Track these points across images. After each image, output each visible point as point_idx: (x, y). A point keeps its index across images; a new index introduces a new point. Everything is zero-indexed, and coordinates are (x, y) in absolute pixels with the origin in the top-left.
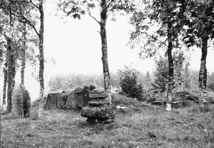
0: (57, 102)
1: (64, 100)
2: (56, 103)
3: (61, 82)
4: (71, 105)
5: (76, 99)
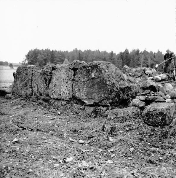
0: (32, 83)
1: (46, 81)
2: (31, 86)
3: (37, 56)
4: (59, 92)
5: (70, 80)
